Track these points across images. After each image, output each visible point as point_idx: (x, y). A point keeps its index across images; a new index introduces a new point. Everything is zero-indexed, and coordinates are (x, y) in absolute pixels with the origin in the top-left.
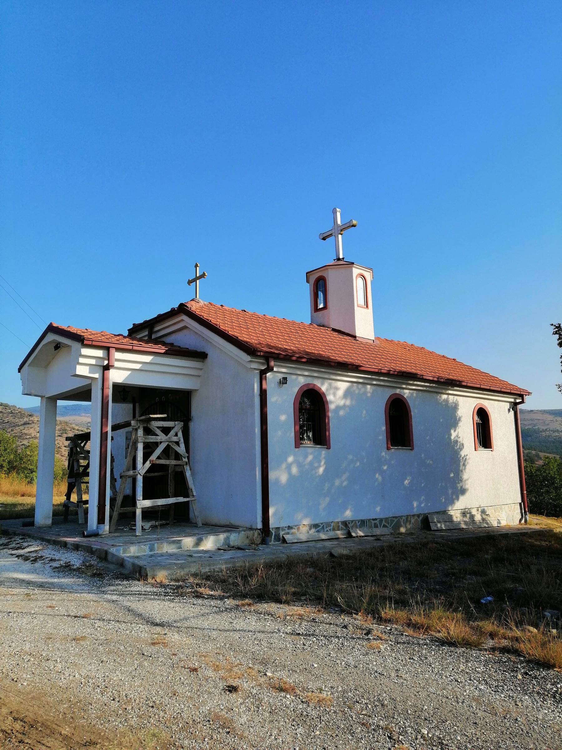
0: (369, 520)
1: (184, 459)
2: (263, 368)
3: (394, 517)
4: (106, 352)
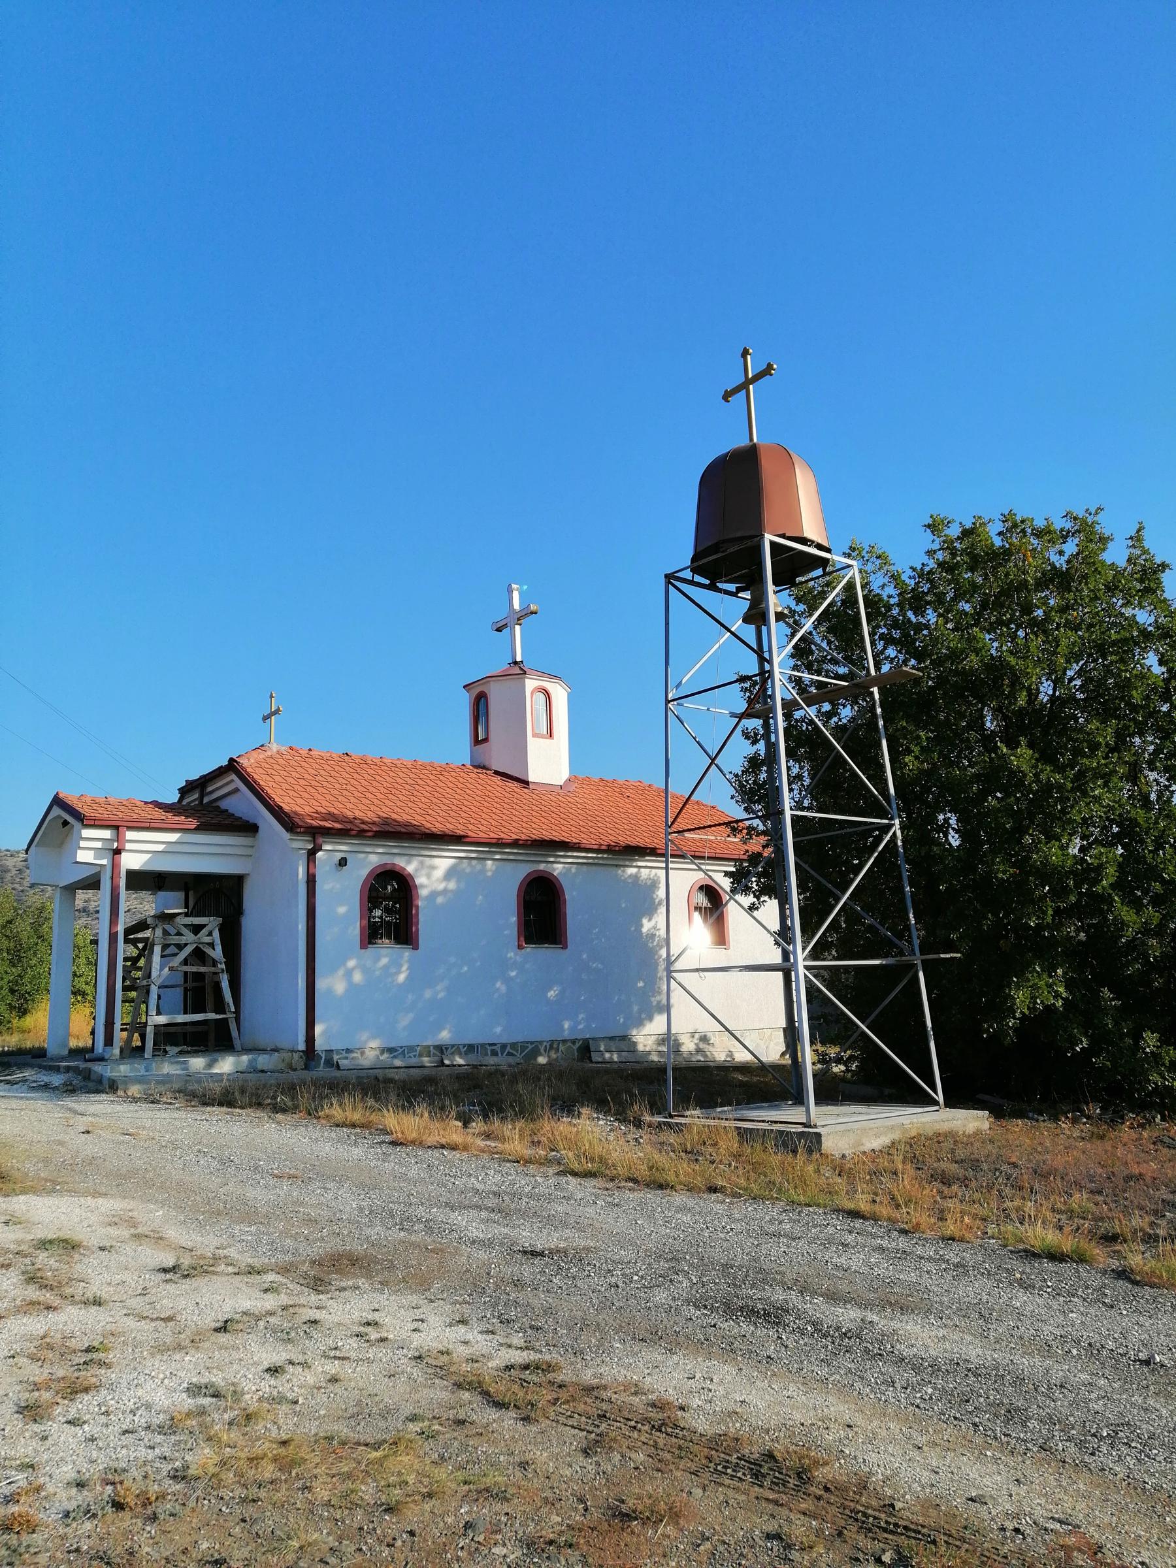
0: (483, 1045)
1: (219, 966)
2: (310, 846)
3: (527, 1042)
4: (115, 832)
